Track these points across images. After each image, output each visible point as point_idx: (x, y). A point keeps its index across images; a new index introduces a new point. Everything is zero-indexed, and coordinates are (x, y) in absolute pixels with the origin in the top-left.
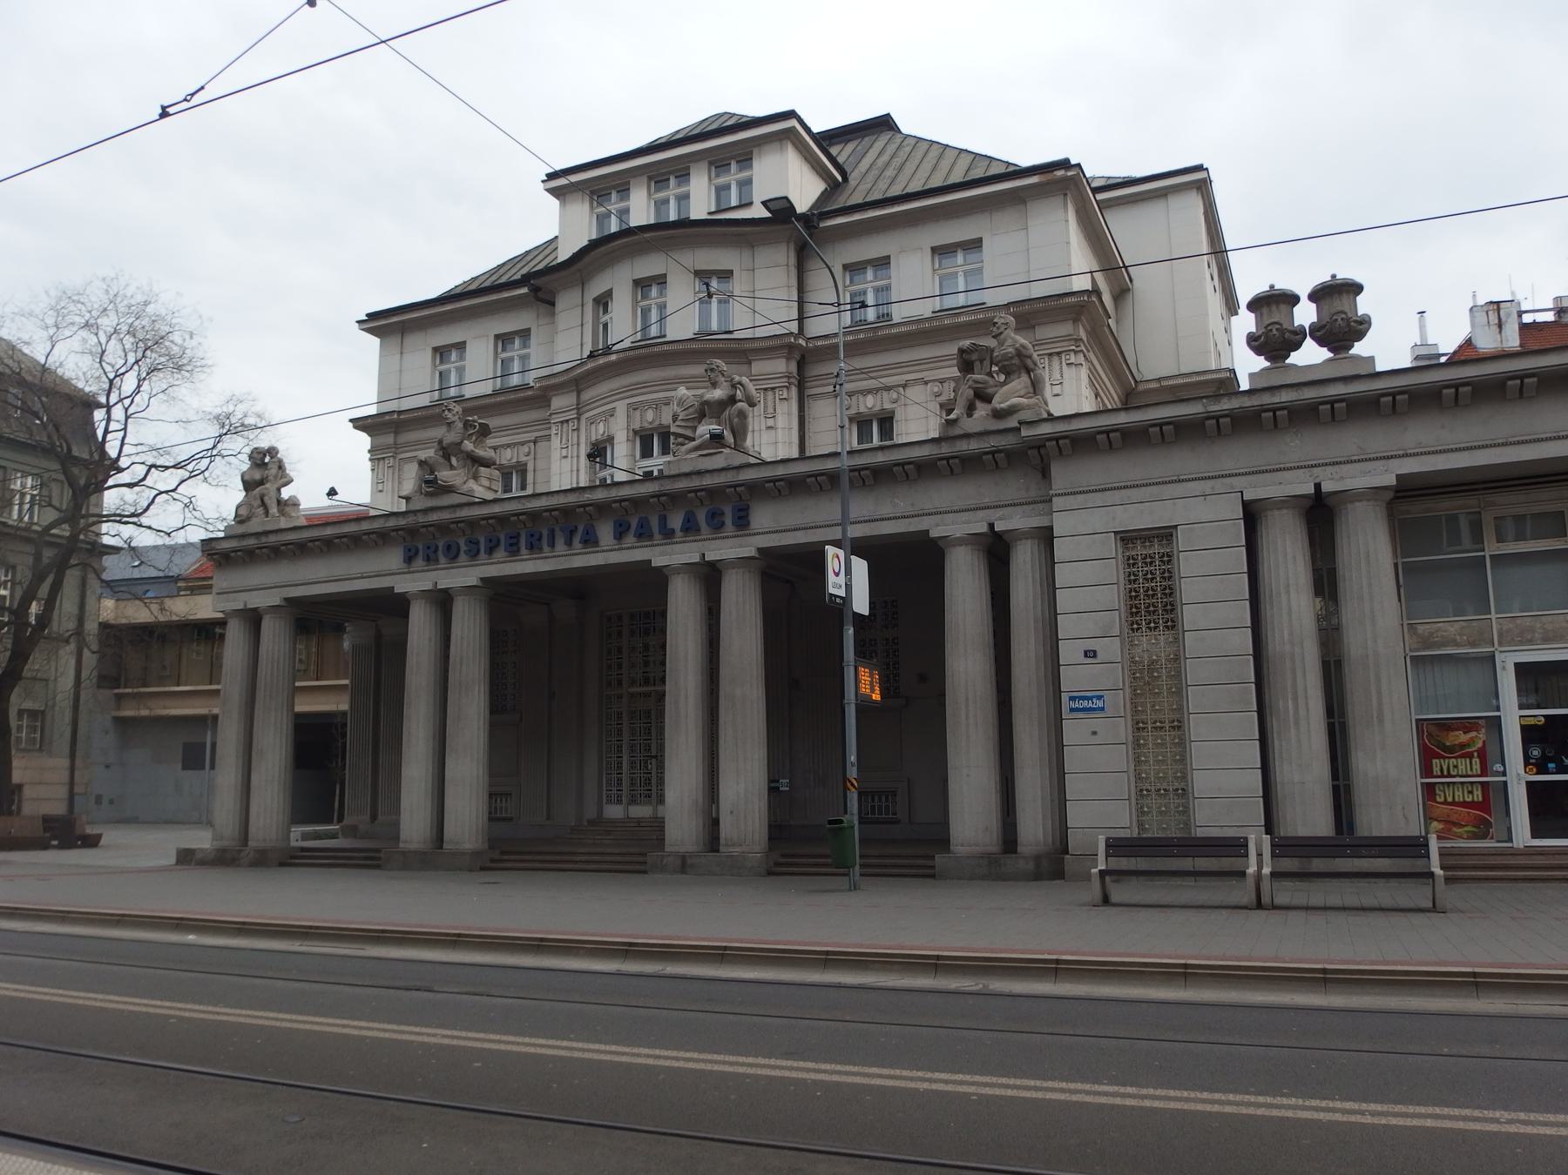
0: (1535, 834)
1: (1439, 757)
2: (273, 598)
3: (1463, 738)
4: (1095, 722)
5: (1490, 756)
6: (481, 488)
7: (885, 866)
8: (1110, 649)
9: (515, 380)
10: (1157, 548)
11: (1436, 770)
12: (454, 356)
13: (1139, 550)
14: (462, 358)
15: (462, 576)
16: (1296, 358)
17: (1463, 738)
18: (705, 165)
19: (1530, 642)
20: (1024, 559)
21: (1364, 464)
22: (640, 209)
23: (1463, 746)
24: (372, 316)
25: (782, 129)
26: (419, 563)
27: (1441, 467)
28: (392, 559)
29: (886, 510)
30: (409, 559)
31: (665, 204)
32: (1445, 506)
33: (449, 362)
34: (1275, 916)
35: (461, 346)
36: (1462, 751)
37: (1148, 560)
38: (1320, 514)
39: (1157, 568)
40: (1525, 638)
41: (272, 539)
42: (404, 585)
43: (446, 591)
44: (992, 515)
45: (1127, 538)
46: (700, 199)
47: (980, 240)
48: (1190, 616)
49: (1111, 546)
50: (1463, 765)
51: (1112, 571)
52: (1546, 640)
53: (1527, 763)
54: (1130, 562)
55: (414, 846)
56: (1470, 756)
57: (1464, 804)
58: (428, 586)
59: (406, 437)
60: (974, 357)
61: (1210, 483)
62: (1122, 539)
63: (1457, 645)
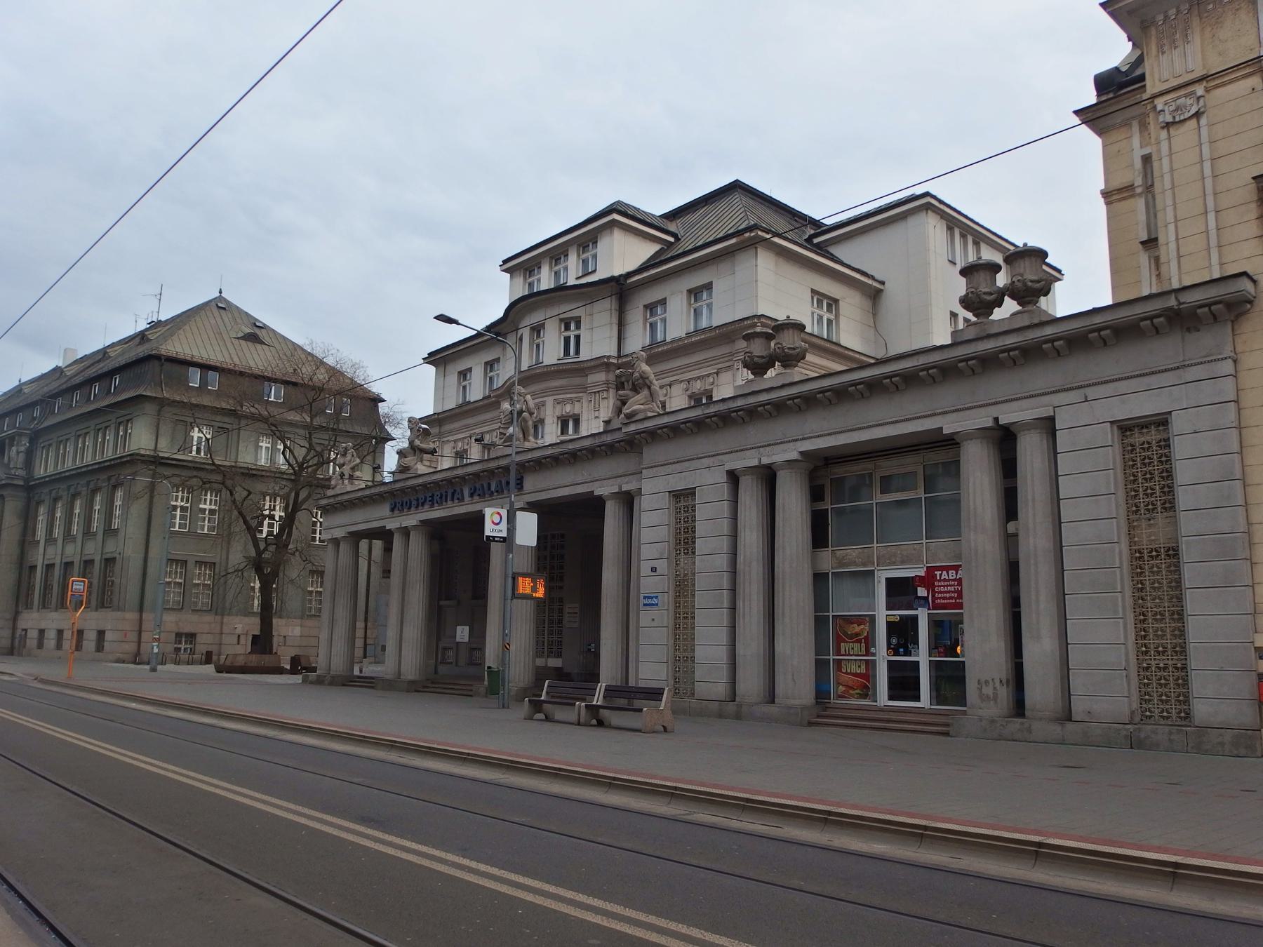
0: (890, 698)
1: (845, 642)
2: (791, 453)
3: (857, 629)
4: (654, 613)
5: (869, 641)
6: (421, 469)
7: (889, 721)
8: (662, 566)
9: (704, 323)
10: (1153, 436)
11: (843, 651)
12: (659, 310)
13: (1138, 438)
14: (710, 296)
15: (411, 520)
16: (998, 314)
17: (857, 629)
18: (575, 248)
19: (894, 563)
20: (1030, 451)
21: (786, 445)
22: (545, 280)
23: (857, 634)
24: (431, 354)
25: (618, 216)
26: (396, 512)
27: (920, 429)
28: (385, 510)
29: (579, 479)
30: (392, 510)
31: (551, 279)
32: (857, 468)
33: (656, 314)
34: (558, 727)
35: (709, 286)
36: (855, 638)
37: (1147, 446)
38: (768, 476)
39: (1155, 453)
40: (890, 561)
41: (339, 498)
42: (391, 525)
43: (628, 493)
44: (994, 411)
45: (1125, 428)
46: (572, 273)
47: (711, 283)
48: (1184, 499)
49: (1108, 435)
50: (856, 646)
51: (1111, 456)
52: (903, 562)
53: (889, 648)
54: (1128, 449)
55: (411, 677)
56: (859, 641)
57: (856, 675)
58: (755, 462)
59: (447, 428)
60: (623, 379)
61: (712, 459)
62: (1120, 428)
63: (856, 565)
